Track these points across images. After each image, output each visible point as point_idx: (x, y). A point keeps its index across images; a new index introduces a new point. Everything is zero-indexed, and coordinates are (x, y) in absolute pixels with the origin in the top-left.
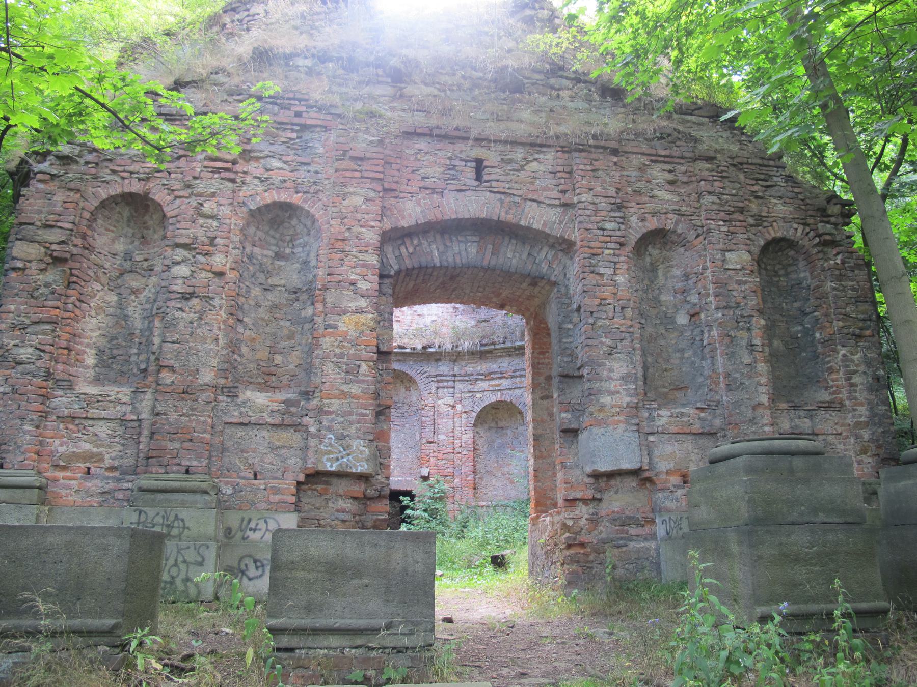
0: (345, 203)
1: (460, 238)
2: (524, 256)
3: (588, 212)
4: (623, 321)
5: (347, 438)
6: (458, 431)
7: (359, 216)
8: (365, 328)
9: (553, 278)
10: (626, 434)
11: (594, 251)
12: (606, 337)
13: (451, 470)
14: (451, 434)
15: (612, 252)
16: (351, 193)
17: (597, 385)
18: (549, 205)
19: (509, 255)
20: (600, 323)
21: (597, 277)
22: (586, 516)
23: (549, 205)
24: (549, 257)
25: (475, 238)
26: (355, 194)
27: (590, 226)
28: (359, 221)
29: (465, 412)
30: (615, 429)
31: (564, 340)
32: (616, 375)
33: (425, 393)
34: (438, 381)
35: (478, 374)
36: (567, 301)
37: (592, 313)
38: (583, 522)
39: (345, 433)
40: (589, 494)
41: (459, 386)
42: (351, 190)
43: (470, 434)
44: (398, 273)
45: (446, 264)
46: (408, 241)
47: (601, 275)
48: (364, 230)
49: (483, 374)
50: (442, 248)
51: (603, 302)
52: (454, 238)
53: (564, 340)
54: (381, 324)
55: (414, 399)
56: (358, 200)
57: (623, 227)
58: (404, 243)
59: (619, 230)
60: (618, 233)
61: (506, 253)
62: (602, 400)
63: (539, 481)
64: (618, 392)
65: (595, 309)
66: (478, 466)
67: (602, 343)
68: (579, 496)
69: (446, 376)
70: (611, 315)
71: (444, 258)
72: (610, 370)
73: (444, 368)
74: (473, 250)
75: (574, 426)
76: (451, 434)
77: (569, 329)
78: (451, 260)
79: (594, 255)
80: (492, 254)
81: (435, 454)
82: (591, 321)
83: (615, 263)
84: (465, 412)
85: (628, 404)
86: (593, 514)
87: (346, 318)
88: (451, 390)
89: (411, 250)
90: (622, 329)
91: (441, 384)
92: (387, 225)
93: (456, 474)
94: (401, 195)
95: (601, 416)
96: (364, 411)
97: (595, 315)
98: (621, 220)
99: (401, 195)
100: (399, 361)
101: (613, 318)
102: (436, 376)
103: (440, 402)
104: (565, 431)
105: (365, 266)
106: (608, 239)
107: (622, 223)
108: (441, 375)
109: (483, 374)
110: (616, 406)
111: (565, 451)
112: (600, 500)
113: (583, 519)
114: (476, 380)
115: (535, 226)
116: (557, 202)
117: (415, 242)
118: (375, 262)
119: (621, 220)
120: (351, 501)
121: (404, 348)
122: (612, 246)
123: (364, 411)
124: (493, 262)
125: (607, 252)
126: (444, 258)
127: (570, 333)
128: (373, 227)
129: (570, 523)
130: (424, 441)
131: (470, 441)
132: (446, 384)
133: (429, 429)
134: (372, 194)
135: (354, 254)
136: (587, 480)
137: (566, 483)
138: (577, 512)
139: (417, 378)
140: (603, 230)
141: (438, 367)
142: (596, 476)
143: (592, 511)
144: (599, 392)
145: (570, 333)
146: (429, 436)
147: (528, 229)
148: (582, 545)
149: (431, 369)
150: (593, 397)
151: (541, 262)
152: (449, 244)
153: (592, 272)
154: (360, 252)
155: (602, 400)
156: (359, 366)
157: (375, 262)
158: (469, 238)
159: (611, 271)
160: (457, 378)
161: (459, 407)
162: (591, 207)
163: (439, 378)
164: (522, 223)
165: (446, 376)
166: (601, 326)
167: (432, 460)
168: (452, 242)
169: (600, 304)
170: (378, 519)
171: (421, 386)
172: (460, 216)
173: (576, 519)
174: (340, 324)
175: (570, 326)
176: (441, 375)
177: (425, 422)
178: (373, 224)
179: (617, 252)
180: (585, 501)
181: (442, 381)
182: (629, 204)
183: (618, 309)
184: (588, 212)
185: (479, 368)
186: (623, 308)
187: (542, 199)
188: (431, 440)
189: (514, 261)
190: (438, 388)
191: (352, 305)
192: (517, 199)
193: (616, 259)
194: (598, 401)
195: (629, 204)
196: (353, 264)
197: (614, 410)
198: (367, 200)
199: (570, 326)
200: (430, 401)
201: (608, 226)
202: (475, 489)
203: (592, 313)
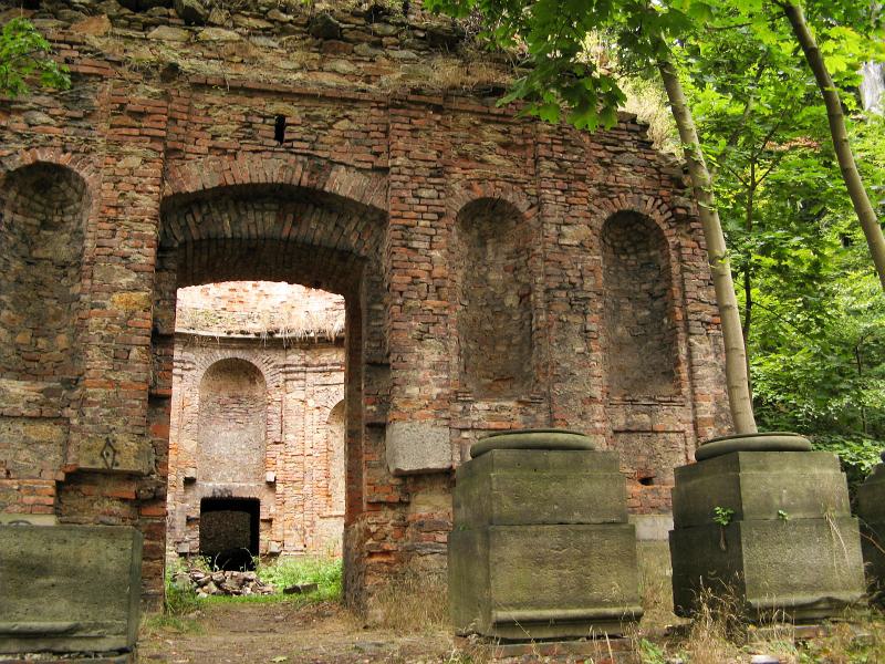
0: (120, 164)
1: (256, 207)
2: (330, 228)
3: (403, 178)
4: (438, 302)
5: (114, 432)
6: (308, 432)
7: (135, 180)
8: (137, 307)
9: (363, 253)
10: (434, 429)
11: (408, 222)
12: (416, 320)
13: (300, 475)
14: (302, 434)
15: (428, 223)
16: (127, 154)
17: (404, 374)
18: (359, 169)
19: (313, 226)
20: (411, 303)
21: (410, 252)
22: (392, 521)
23: (359, 169)
24: (360, 228)
25: (274, 206)
26: (131, 154)
27: (404, 193)
28: (135, 185)
29: (318, 408)
30: (421, 423)
31: (373, 323)
32: (426, 364)
33: (271, 386)
34: (286, 373)
35: (333, 364)
36: (378, 279)
37: (401, 293)
38: (389, 527)
39: (112, 426)
40: (395, 496)
41: (311, 377)
42: (128, 149)
43: (323, 433)
44: (184, 244)
45: (238, 235)
46: (195, 211)
47: (416, 250)
48: (141, 196)
49: (338, 364)
50: (234, 217)
51: (415, 280)
52: (249, 206)
53: (373, 323)
54: (161, 303)
55: (259, 394)
56: (135, 162)
57: (442, 195)
58: (191, 212)
59: (439, 198)
60: (437, 202)
61: (308, 224)
62: (407, 392)
63: (353, 483)
64: (428, 382)
65: (404, 288)
66: (332, 470)
67: (411, 327)
68: (383, 499)
69: (296, 366)
70: (423, 295)
71: (237, 228)
72: (420, 357)
73: (294, 358)
74: (270, 219)
75: (381, 420)
76: (302, 434)
77: (380, 311)
78: (244, 230)
79: (407, 227)
80: (294, 224)
81: (283, 457)
82: (399, 301)
83: (432, 236)
84: (318, 408)
85: (438, 395)
86: (400, 519)
87: (116, 296)
88: (301, 383)
89: (199, 219)
90: (436, 311)
91: (289, 376)
92: (169, 191)
93: (307, 479)
94: (188, 156)
95: (407, 408)
96: (133, 402)
97: (405, 294)
98: (441, 187)
99: (188, 156)
100: (241, 348)
101: (426, 299)
102: (285, 366)
103: (288, 396)
104: (371, 426)
105: (141, 237)
106: (424, 208)
107: (442, 191)
108: (290, 365)
109: (338, 364)
110: (424, 398)
111: (371, 449)
112: (408, 504)
113: (389, 525)
114: (331, 371)
115: (342, 193)
116: (369, 166)
117: (204, 210)
118: (153, 233)
119: (441, 187)
120: (119, 503)
121: (248, 333)
122: (430, 216)
123: (133, 402)
124: (293, 234)
125: (422, 223)
126: (237, 228)
127: (380, 315)
128: (151, 192)
129: (373, 528)
130: (270, 441)
131: (323, 442)
132: (296, 375)
133: (276, 427)
134: (151, 155)
135: (127, 222)
136: (393, 481)
137: (369, 484)
138: (382, 517)
139: (264, 369)
140: (420, 198)
141: (286, 356)
142: (400, 475)
143: (398, 515)
144: (406, 381)
145: (380, 315)
146: (275, 435)
147: (333, 195)
148: (387, 553)
149: (279, 358)
150: (398, 388)
151: (349, 234)
152: (243, 213)
153: (404, 246)
154: (135, 221)
155: (407, 392)
156: (129, 352)
157: (153, 233)
158: (267, 205)
159: (427, 245)
160: (308, 369)
161: (311, 403)
162: (406, 171)
163: (287, 369)
164: (327, 189)
165: (296, 366)
166: (411, 307)
167: (278, 462)
168: (247, 210)
169: (412, 283)
170: (154, 524)
171: (268, 378)
172: (255, 181)
173: (381, 525)
174: (108, 303)
175: (380, 307)
176: (290, 365)
177: (271, 420)
178: (150, 188)
179: (434, 223)
180: (391, 505)
181: (291, 372)
182: (451, 169)
183: (432, 289)
184: (403, 178)
185: (334, 357)
186: (437, 288)
187: (351, 162)
188: (278, 440)
189: (318, 233)
190: (286, 380)
191: (124, 281)
192: (323, 162)
193: (433, 232)
194: (404, 392)
195: (451, 169)
196: (126, 235)
197: (422, 403)
198: (145, 161)
199: (380, 307)
200: (277, 396)
201: (425, 193)
202: (329, 496)
203: (401, 293)
